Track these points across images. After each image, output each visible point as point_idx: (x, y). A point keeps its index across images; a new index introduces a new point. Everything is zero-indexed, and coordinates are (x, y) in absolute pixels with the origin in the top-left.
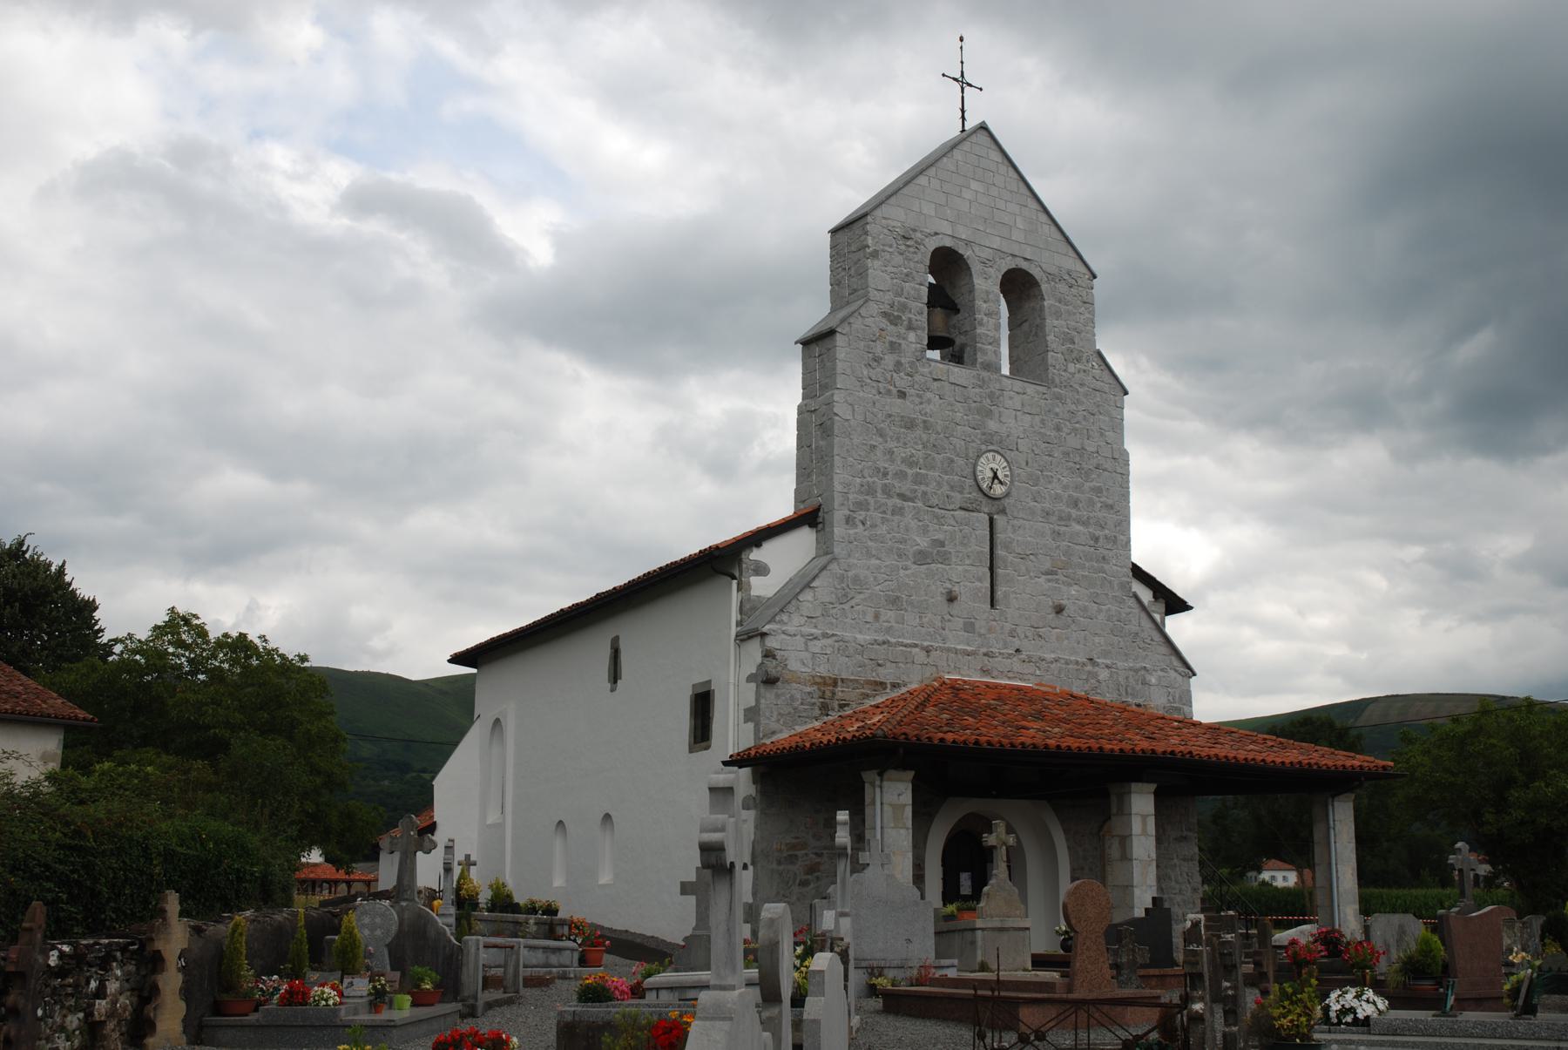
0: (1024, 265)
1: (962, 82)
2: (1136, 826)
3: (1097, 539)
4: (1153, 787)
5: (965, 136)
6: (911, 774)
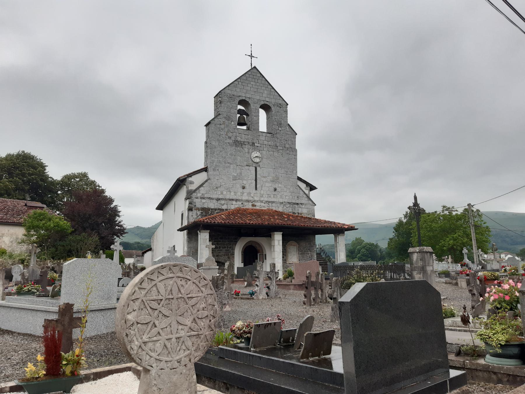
1: (251, 56)
2: (276, 243)
3: (287, 172)
5: (252, 69)
6: (209, 231)
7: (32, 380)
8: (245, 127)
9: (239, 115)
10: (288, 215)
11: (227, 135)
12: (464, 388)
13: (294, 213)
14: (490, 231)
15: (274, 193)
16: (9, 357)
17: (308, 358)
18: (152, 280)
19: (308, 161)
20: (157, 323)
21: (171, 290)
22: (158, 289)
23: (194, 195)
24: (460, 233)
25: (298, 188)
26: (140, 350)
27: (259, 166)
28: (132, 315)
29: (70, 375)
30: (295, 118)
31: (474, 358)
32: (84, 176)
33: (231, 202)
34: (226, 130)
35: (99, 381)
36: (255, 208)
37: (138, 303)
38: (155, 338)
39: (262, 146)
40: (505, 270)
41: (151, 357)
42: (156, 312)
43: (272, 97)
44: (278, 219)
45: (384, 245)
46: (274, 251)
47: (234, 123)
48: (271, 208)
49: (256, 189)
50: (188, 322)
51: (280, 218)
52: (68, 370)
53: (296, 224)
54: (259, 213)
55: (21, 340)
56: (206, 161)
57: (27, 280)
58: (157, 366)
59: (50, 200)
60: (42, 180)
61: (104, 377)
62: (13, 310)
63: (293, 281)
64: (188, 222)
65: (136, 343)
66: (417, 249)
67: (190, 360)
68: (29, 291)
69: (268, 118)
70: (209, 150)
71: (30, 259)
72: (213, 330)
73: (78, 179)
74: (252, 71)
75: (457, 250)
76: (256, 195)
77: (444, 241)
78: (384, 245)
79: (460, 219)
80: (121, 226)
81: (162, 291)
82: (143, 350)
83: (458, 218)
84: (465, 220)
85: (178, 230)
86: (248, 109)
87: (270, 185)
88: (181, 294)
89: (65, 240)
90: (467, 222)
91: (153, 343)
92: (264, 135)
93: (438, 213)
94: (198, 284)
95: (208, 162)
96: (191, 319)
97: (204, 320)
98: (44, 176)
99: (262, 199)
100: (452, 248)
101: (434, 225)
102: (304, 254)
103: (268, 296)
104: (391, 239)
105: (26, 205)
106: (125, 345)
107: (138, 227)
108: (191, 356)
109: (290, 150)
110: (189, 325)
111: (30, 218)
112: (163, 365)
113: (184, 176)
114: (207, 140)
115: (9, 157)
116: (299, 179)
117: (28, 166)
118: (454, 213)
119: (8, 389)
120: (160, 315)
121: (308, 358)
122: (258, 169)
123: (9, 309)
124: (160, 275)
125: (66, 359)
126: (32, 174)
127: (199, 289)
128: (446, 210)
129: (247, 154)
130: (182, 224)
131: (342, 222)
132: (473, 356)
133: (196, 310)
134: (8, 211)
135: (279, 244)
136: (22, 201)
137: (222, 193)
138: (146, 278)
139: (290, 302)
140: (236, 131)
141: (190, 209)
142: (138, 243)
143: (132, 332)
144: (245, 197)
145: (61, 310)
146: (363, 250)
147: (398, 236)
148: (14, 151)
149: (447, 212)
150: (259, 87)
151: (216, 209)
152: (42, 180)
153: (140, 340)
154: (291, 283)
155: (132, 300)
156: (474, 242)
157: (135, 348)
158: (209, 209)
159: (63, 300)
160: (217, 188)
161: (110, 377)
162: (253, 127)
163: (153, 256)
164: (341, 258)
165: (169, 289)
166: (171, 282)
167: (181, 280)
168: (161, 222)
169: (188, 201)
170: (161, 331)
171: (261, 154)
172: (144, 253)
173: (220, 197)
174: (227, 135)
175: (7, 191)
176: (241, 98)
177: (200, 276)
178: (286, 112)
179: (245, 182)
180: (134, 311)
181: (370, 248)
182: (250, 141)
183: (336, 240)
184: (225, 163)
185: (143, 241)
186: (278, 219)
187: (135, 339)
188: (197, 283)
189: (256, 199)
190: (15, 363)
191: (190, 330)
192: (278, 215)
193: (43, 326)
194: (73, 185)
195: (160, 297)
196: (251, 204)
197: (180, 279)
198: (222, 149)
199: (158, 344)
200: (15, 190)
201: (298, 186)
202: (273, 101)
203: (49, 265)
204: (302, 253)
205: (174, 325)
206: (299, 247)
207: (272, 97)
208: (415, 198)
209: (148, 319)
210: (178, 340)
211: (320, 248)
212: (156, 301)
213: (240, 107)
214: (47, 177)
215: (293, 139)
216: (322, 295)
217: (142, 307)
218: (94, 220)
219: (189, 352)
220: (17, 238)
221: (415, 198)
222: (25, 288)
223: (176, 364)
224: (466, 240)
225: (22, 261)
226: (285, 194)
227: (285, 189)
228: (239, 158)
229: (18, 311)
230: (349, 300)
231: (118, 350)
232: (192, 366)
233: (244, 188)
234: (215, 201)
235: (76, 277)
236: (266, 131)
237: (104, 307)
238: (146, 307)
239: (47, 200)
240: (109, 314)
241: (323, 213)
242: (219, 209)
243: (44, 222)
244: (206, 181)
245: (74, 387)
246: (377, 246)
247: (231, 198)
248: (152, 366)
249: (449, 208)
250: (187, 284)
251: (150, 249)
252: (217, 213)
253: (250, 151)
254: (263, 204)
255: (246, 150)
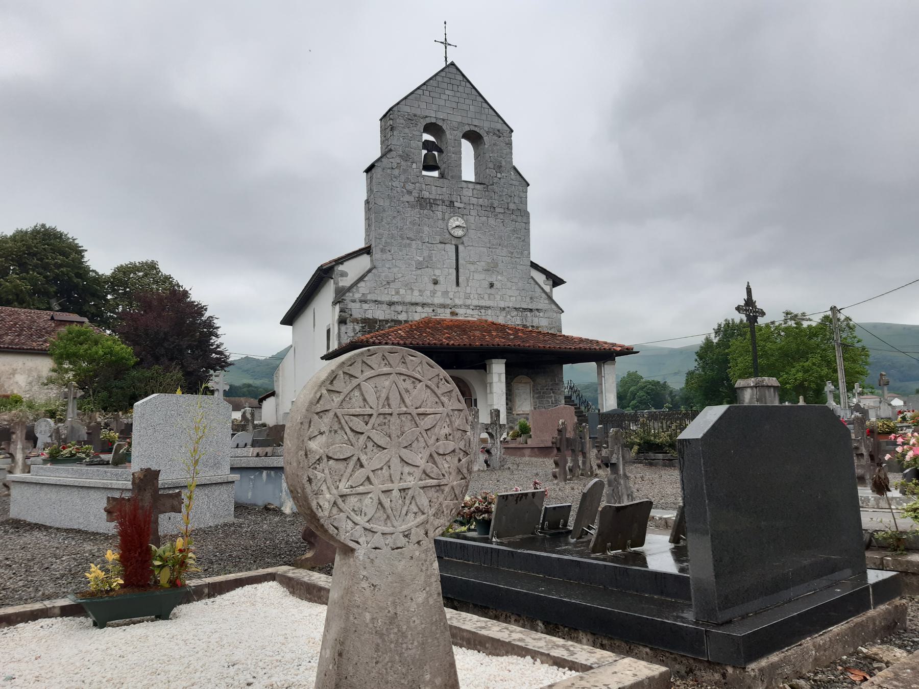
0: (473, 128)
1: (446, 44)
2: (495, 378)
4: (504, 361)
5: (447, 66)
7: (99, 595)
8: (435, 174)
9: (424, 152)
10: (516, 330)
11: (404, 187)
12: (897, 601)
13: (524, 326)
14: (867, 355)
15: (489, 291)
16: (46, 565)
17: (604, 552)
18: (352, 376)
19: (548, 237)
20: (363, 458)
21: (387, 398)
22: (363, 395)
23: (349, 296)
24: (816, 359)
25: (532, 282)
26: (335, 510)
27: (463, 243)
28: (317, 443)
29: (167, 586)
30: (523, 157)
31: (899, 552)
32: (151, 268)
33: (413, 308)
34: (403, 178)
35: (219, 599)
36: (455, 318)
37: (328, 419)
38: (361, 487)
39: (468, 207)
40: (904, 419)
41: (356, 524)
42: (362, 438)
43: (484, 117)
44: (497, 336)
45: (677, 384)
46: (491, 393)
47: (417, 167)
48: (484, 318)
49: (458, 284)
50: (420, 459)
51: (500, 334)
52: (164, 577)
53: (530, 344)
54: (463, 327)
55: (64, 539)
56: (368, 235)
57: (65, 441)
58: (368, 543)
59: (93, 310)
60: (78, 275)
61: (228, 591)
62: (45, 488)
63: (529, 441)
64: (340, 343)
65: (328, 496)
66: (752, 382)
67: (426, 534)
68: (73, 455)
69: (477, 157)
70: (373, 216)
71: (66, 411)
72: (465, 478)
73: (141, 274)
74: (447, 70)
75: (808, 388)
76: (457, 294)
77: (787, 373)
78: (677, 384)
79: (816, 335)
80: (221, 353)
81: (372, 399)
82: (341, 511)
83: (813, 332)
84: (825, 335)
85: (322, 358)
86: (442, 140)
87: (482, 276)
88: (406, 406)
89: (124, 379)
90: (829, 339)
91: (359, 497)
92: (471, 186)
93: (777, 324)
94: (436, 389)
95: (373, 235)
96: (426, 454)
97: (448, 458)
98: (81, 268)
99: (468, 302)
100: (801, 385)
101: (769, 345)
102: (543, 397)
103: (488, 465)
104: (690, 374)
105: (52, 318)
106: (306, 498)
107: (247, 358)
108: (428, 526)
109: (518, 213)
110: (422, 467)
111: (61, 339)
112: (377, 540)
113: (330, 262)
114: (369, 197)
115: (20, 237)
116: (534, 266)
117: (54, 251)
118: (805, 324)
119: (57, 611)
120: (370, 444)
121: (604, 552)
122: (461, 248)
123: (38, 487)
124: (365, 368)
125: (160, 556)
126: (61, 266)
127: (437, 400)
128: (791, 319)
129: (440, 222)
130: (328, 348)
131: (610, 340)
132: (896, 550)
133: (434, 438)
134: (22, 330)
135: (500, 380)
136: (45, 312)
137: (397, 293)
138: (341, 372)
139: (529, 475)
140: (421, 180)
141: (342, 321)
142: (249, 386)
143: (320, 475)
144: (438, 300)
145: (137, 481)
146: (641, 393)
147: (703, 368)
148: (27, 225)
149: (792, 323)
150: (462, 100)
151: (387, 321)
152: (78, 275)
153: (334, 491)
154: (525, 446)
155: (317, 413)
156: (841, 375)
157: (326, 506)
158: (375, 321)
159: (137, 465)
160: (388, 283)
161: (239, 591)
162: (450, 173)
163: (277, 405)
164: (609, 402)
165: (384, 395)
166: (387, 383)
167: (404, 380)
168: (287, 350)
169: (337, 307)
170: (371, 475)
171: (466, 221)
172: (261, 401)
173: (395, 299)
174: (404, 187)
175: (17, 295)
176: (428, 121)
177: (438, 375)
178: (510, 144)
179: (437, 272)
180: (321, 433)
181: (652, 390)
182: (446, 198)
183: (599, 372)
184: (403, 239)
185: (257, 383)
186: (497, 336)
187: (324, 488)
188: (434, 387)
189: (458, 302)
190: (58, 576)
191: (424, 476)
192: (496, 330)
193: (106, 510)
194: (134, 284)
195: (368, 411)
196: (448, 311)
197: (403, 377)
198: (395, 214)
199: (367, 500)
200: (36, 291)
201: (532, 278)
202: (486, 125)
203: (99, 420)
204: (540, 395)
205: (395, 461)
206: (534, 386)
207: (484, 117)
208: (749, 291)
209: (347, 451)
210: (403, 494)
211: (571, 388)
212: (361, 418)
213: (427, 137)
214: (87, 270)
215: (522, 195)
216: (584, 463)
217: (336, 427)
218: (173, 343)
219: (423, 517)
220: (39, 377)
221: (749, 291)
222: (65, 452)
223: (402, 541)
224: (825, 371)
225: (52, 414)
226: (510, 293)
227: (509, 284)
228: (426, 229)
229: (54, 490)
230: (700, 436)
231: (239, 553)
232: (429, 544)
233: (436, 283)
234: (385, 307)
235: (158, 428)
236: (473, 180)
237: (209, 480)
238: (342, 428)
239: (88, 311)
240: (217, 493)
241: (578, 321)
242: (392, 321)
243: (85, 346)
244: (369, 271)
245: (175, 610)
246: (664, 386)
247: (413, 301)
248: (358, 542)
249: (796, 316)
250: (415, 388)
251: (273, 394)
252: (390, 327)
253: (447, 217)
254: (469, 312)
255: (439, 215)
